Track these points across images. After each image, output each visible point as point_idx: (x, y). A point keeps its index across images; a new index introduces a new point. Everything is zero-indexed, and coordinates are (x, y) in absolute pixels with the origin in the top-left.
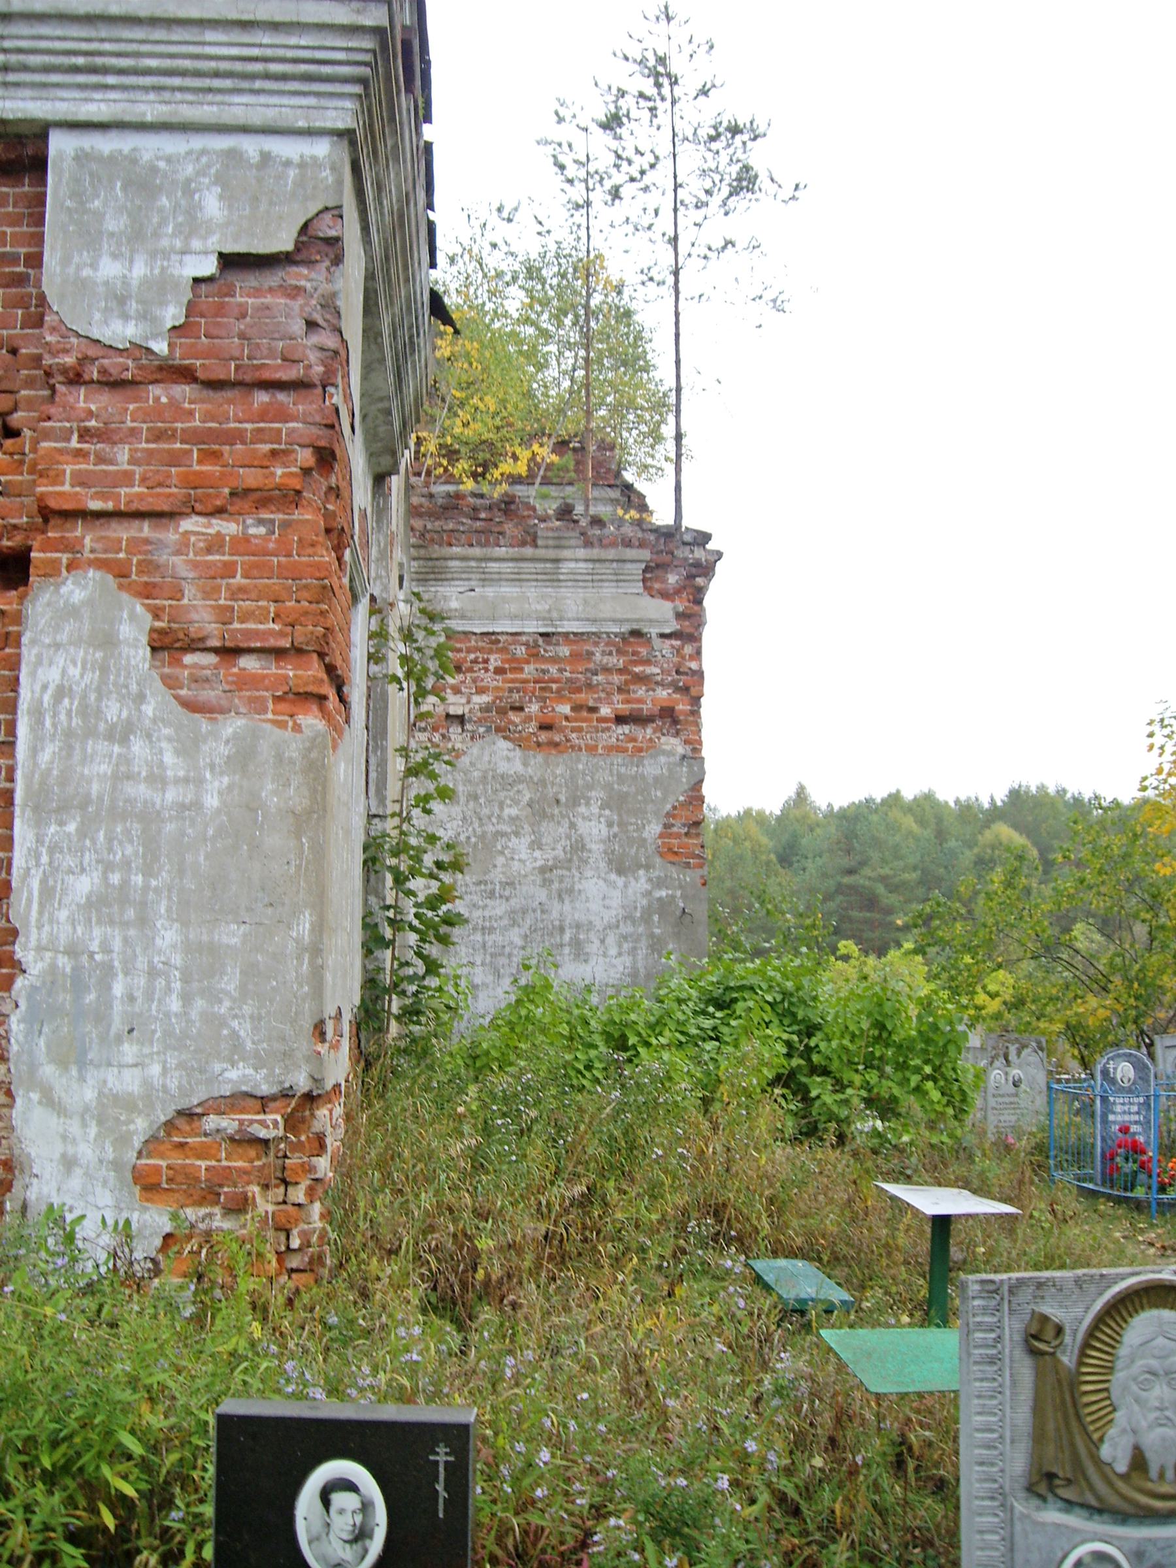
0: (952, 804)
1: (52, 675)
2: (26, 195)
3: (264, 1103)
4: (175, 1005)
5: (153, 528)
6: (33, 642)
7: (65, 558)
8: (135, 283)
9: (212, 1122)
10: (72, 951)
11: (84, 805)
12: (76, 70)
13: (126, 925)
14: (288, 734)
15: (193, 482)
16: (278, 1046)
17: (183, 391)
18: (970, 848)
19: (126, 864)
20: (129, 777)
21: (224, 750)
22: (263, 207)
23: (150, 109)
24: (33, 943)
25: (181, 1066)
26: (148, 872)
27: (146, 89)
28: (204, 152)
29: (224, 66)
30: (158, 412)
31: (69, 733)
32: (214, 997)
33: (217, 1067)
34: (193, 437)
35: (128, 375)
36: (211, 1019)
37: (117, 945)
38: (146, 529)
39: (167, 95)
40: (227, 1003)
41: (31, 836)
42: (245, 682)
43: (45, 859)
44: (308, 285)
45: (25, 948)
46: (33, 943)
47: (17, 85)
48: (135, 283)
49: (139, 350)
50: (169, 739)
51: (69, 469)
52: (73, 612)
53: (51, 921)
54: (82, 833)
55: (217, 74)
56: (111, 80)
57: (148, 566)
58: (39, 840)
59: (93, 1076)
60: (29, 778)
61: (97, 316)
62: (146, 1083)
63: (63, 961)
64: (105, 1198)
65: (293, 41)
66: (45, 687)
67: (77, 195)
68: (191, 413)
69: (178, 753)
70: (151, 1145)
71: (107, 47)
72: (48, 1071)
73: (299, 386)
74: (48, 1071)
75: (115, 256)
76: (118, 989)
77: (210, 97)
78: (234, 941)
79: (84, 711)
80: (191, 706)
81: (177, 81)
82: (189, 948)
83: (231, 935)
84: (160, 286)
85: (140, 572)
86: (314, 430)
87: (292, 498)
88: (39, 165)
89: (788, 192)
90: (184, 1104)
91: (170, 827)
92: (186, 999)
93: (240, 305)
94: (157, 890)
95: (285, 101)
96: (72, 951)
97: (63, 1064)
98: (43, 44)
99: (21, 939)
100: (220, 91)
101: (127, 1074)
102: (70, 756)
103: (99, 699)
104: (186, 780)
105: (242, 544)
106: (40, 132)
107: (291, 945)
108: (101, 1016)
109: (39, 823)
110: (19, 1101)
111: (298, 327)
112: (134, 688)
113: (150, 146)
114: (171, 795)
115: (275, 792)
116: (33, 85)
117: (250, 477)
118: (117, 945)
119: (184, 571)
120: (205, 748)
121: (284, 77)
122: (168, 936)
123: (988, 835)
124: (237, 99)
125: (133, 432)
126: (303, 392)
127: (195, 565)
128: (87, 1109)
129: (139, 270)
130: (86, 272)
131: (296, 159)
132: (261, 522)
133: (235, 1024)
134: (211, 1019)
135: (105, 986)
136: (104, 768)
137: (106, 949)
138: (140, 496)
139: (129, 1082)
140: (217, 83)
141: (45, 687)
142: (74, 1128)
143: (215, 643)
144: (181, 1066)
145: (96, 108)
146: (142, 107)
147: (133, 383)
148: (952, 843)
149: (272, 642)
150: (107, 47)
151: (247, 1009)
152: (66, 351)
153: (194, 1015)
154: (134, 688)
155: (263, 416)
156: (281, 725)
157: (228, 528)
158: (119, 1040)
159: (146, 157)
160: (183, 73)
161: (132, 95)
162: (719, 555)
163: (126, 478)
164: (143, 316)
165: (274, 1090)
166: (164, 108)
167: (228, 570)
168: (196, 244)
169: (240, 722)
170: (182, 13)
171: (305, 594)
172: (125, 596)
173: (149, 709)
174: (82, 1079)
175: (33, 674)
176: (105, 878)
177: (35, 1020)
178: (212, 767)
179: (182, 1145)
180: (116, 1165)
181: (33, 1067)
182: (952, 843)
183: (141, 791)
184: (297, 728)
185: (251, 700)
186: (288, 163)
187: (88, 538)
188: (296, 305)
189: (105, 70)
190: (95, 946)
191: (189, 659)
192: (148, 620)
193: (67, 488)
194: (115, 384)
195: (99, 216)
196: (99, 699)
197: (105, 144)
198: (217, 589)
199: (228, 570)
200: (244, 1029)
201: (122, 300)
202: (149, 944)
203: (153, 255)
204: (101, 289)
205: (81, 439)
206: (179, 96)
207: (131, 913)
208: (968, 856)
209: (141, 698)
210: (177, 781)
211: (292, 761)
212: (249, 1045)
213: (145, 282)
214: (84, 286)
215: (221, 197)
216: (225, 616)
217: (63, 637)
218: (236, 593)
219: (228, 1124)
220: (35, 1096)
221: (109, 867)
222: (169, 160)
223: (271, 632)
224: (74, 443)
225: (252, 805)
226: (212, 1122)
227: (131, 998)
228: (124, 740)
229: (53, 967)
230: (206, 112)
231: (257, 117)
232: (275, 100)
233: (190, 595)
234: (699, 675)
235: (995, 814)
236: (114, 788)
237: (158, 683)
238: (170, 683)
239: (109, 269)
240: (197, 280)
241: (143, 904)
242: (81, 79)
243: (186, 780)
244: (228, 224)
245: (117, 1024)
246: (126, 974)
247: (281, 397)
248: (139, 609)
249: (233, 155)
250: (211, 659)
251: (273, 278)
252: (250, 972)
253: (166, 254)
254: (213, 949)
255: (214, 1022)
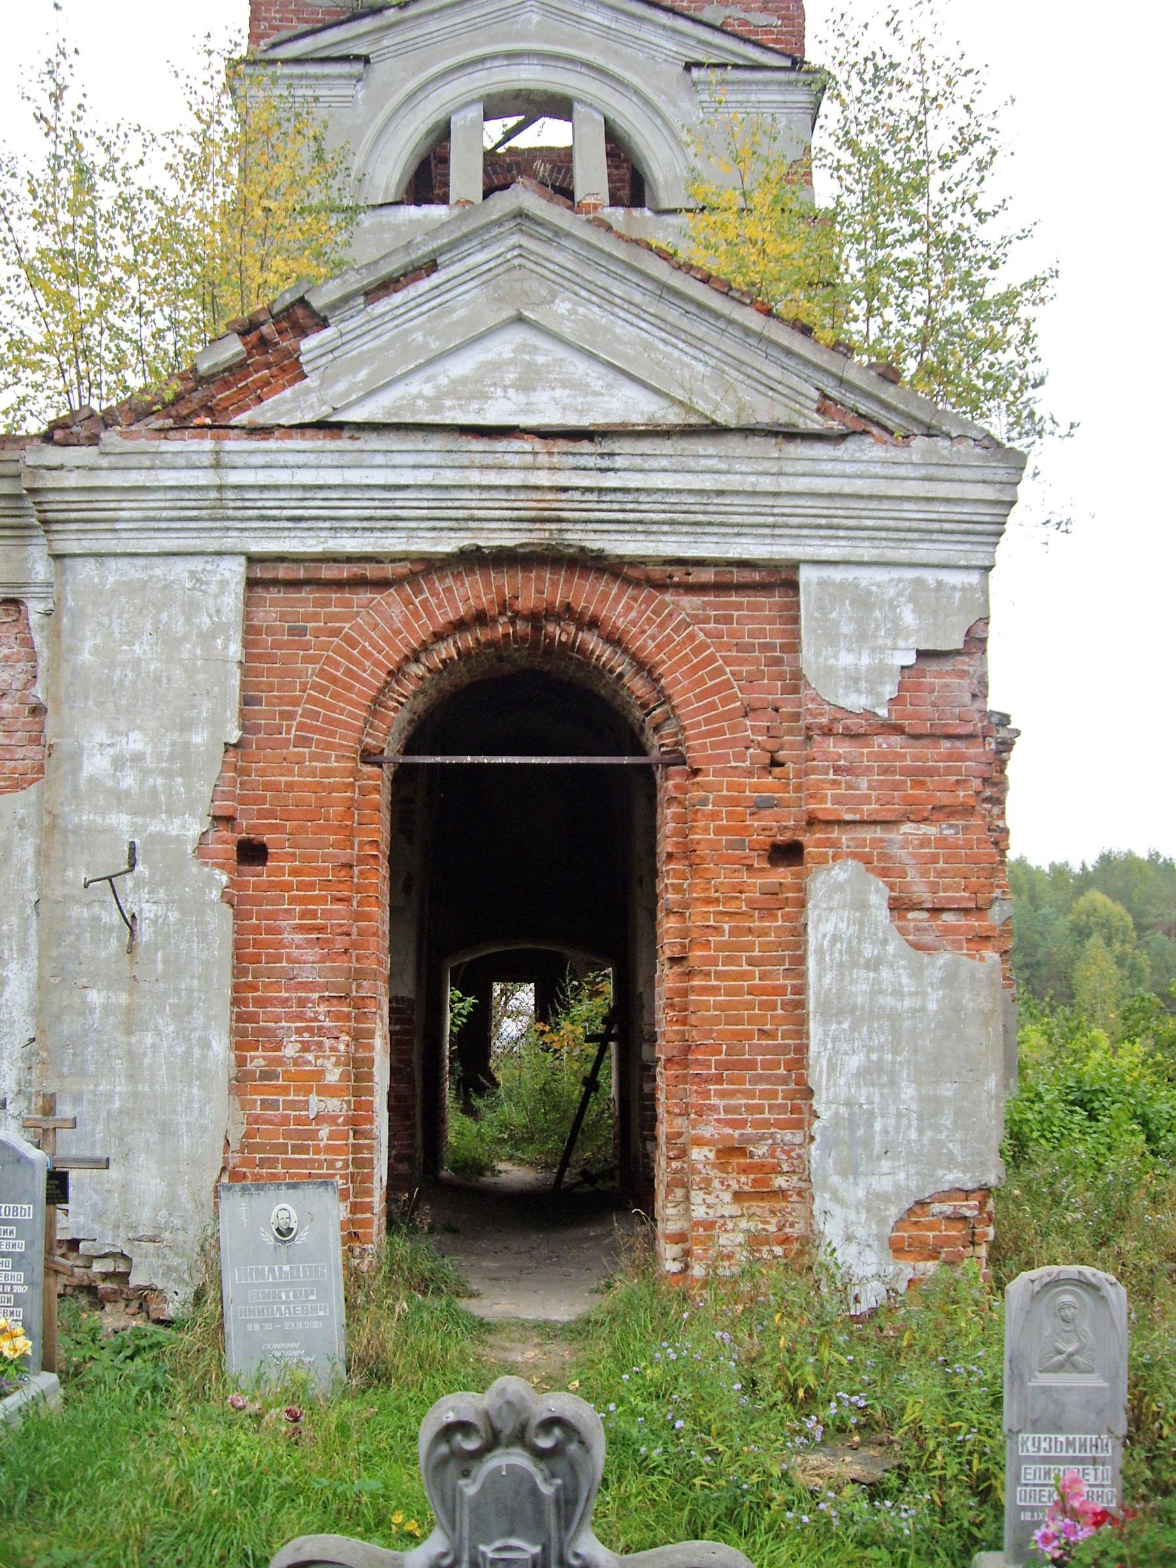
0: (1047, 870)
1: (829, 928)
2: (776, 603)
3: (967, 1194)
4: (913, 1135)
5: (883, 831)
6: (815, 907)
7: (831, 851)
8: (863, 669)
9: (936, 1208)
10: (848, 1104)
11: (852, 1012)
12: (820, 527)
13: (882, 1086)
14: (977, 963)
15: (907, 801)
16: (977, 1158)
17: (897, 740)
18: (1065, 914)
19: (881, 1048)
20: (880, 992)
21: (939, 974)
22: (941, 618)
23: (866, 552)
24: (824, 1100)
25: (918, 1173)
26: (895, 1052)
27: (863, 539)
28: (900, 580)
29: (915, 525)
30: (883, 756)
31: (841, 965)
32: (938, 1129)
33: (940, 1173)
34: (905, 771)
35: (862, 731)
36: (936, 1143)
37: (877, 1098)
38: (878, 832)
39: (876, 543)
40: (945, 1133)
41: (820, 1031)
42: (948, 930)
43: (830, 1046)
44: (971, 670)
45: (819, 1102)
46: (824, 1100)
47: (780, 536)
48: (863, 669)
49: (869, 714)
50: (905, 968)
51: (829, 793)
52: (839, 887)
53: (835, 1085)
54: (853, 1029)
55: (909, 530)
56: (841, 533)
57: (883, 857)
58: (826, 1034)
59: (862, 1181)
60: (817, 994)
61: (841, 691)
62: (896, 1185)
63: (843, 1110)
64: (871, 1257)
65: (958, 509)
66: (824, 936)
67: (821, 608)
68: (904, 756)
69: (910, 976)
70: (899, 1224)
71: (840, 512)
72: (835, 1179)
73: (970, 737)
74: (835, 1179)
75: (849, 651)
76: (878, 1126)
77: (904, 544)
78: (950, 1094)
79: (850, 951)
80: (917, 946)
81: (883, 534)
82: (922, 1099)
83: (947, 1090)
84: (879, 672)
85: (879, 860)
86: (982, 767)
87: (967, 810)
88: (792, 586)
89: (1064, 429)
90: (919, 1197)
91: (907, 1023)
92: (920, 1130)
93: (931, 684)
94: (900, 1063)
95: (951, 547)
96: (848, 1104)
97: (844, 1174)
98: (799, 511)
99: (816, 1097)
100: (910, 540)
101: (884, 1179)
102: (842, 980)
103: (859, 943)
104: (916, 994)
105: (941, 842)
106: (795, 565)
107: (984, 1095)
108: (867, 1143)
109: (825, 1023)
110: (817, 1199)
111: (967, 698)
112: (881, 935)
113: (866, 576)
114: (907, 1003)
115: (971, 1000)
116: (791, 536)
117: (944, 798)
118: (877, 1098)
119: (907, 860)
120: (927, 973)
121: (952, 532)
122: (908, 1092)
123: (1083, 902)
124: (921, 546)
125: (869, 768)
126: (971, 741)
127: (914, 855)
128: (859, 1202)
129: (865, 660)
130: (831, 661)
131: (959, 586)
132: (951, 826)
133: (951, 1145)
134: (936, 1143)
135: (870, 1125)
136: (865, 987)
137: (870, 1101)
138: (877, 811)
139: (884, 1184)
140: (909, 535)
141: (824, 936)
142: (852, 1215)
143: (929, 906)
144: (918, 1173)
145: (831, 551)
146: (861, 551)
147: (865, 735)
148: (1046, 910)
149: (964, 905)
150: (840, 512)
151: (958, 1136)
152: (822, 714)
153: (925, 1141)
154: (881, 935)
155: (949, 757)
156: (972, 957)
157: (930, 830)
158: (879, 1158)
159: (864, 583)
160: (888, 529)
161: (854, 543)
162: (1018, 733)
163: (866, 799)
164: (870, 692)
165: (976, 1186)
166: (875, 551)
167: (934, 859)
168: (901, 643)
169: (948, 956)
170: (890, 493)
171: (982, 873)
172: (872, 877)
173: (890, 949)
174: (856, 1184)
175: (816, 927)
176: (868, 1057)
177: (826, 1148)
178: (932, 984)
179: (916, 1223)
180: (878, 1237)
181: (825, 1178)
182: (1046, 910)
183: (887, 1001)
184: (982, 959)
185: (954, 942)
186: (954, 588)
187: (844, 838)
188: (965, 682)
189: (838, 528)
190: (863, 1100)
191: (910, 915)
192: (887, 892)
193: (829, 805)
194: (851, 735)
195: (836, 623)
196: (859, 943)
197: (837, 575)
198: (927, 871)
199: (934, 859)
200: (955, 1148)
201: (856, 680)
202: (897, 1097)
203: (874, 650)
204: (842, 673)
205: (835, 772)
206: (884, 543)
207: (885, 1078)
208: (1063, 924)
209: (885, 942)
210: (911, 994)
211: (981, 980)
212: (960, 1159)
213: (870, 669)
214: (830, 671)
215: (914, 611)
216: (934, 888)
217: (834, 903)
218: (940, 874)
219: (947, 1208)
220: (827, 1196)
221: (870, 1050)
222: (878, 585)
223: (962, 898)
224: (831, 776)
225: (957, 1008)
226: (936, 1208)
227: (886, 1132)
228: (876, 969)
229: (837, 1113)
230: (902, 554)
231: (934, 558)
232: (944, 546)
233: (912, 875)
234: (1005, 831)
235: (1086, 880)
236: (871, 999)
237: (896, 933)
238: (903, 931)
239: (846, 659)
240: (903, 667)
241: (892, 1073)
242: (822, 532)
243: (916, 994)
244: (920, 630)
245: (878, 1149)
246: (883, 1116)
247: (958, 743)
248: (881, 884)
249: (918, 583)
250: (925, 915)
251: (947, 665)
252: (960, 1113)
253: (882, 649)
254: (936, 1099)
255: (938, 1144)
